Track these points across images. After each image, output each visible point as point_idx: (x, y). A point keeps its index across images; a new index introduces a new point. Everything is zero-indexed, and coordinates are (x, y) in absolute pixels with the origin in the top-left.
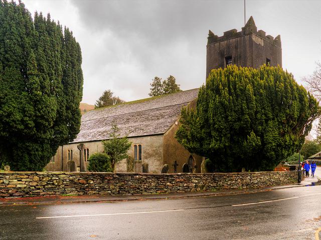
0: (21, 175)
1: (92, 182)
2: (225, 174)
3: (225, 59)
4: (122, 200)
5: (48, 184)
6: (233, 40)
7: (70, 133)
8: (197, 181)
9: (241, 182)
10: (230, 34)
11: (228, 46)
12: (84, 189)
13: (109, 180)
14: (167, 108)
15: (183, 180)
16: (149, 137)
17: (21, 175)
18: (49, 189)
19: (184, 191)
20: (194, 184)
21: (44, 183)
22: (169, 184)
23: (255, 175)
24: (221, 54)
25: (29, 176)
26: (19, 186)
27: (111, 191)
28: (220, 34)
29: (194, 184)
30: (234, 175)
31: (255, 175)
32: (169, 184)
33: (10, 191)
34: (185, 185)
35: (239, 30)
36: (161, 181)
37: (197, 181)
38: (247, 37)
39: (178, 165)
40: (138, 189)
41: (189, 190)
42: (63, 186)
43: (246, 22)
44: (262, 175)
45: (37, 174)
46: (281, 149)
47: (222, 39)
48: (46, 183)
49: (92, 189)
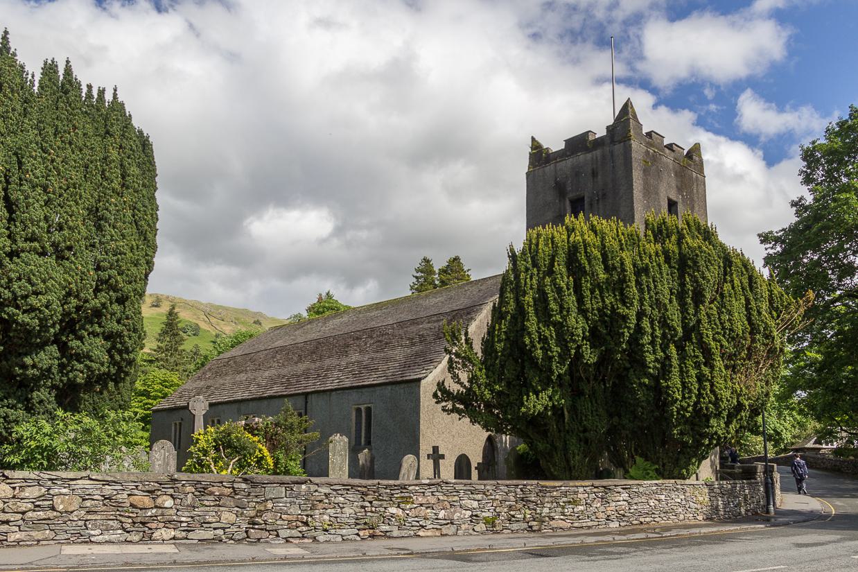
2: (557, 483)
3: (568, 203)
4: (126, 564)
6: (582, 157)
7: (113, 362)
8: (475, 504)
9: (602, 509)
10: (578, 144)
11: (577, 172)
12: (143, 524)
13: (220, 497)
14: (435, 318)
15: (433, 500)
16: (389, 388)
18: (36, 524)
19: (438, 533)
20: (469, 513)
21: (24, 506)
22: (393, 510)
23: (641, 489)
24: (560, 189)
27: (224, 529)
28: (555, 144)
29: (469, 513)
30: (583, 489)
31: (641, 489)
32: (393, 510)
34: (442, 514)
35: (601, 132)
36: (371, 502)
37: (475, 504)
38: (618, 148)
39: (442, 457)
40: (306, 524)
41: (452, 529)
42: (83, 512)
43: (617, 113)
44: (662, 489)
45: (7, 478)
46: (6, 168)
47: (561, 155)
48: (30, 506)
49: (168, 523)
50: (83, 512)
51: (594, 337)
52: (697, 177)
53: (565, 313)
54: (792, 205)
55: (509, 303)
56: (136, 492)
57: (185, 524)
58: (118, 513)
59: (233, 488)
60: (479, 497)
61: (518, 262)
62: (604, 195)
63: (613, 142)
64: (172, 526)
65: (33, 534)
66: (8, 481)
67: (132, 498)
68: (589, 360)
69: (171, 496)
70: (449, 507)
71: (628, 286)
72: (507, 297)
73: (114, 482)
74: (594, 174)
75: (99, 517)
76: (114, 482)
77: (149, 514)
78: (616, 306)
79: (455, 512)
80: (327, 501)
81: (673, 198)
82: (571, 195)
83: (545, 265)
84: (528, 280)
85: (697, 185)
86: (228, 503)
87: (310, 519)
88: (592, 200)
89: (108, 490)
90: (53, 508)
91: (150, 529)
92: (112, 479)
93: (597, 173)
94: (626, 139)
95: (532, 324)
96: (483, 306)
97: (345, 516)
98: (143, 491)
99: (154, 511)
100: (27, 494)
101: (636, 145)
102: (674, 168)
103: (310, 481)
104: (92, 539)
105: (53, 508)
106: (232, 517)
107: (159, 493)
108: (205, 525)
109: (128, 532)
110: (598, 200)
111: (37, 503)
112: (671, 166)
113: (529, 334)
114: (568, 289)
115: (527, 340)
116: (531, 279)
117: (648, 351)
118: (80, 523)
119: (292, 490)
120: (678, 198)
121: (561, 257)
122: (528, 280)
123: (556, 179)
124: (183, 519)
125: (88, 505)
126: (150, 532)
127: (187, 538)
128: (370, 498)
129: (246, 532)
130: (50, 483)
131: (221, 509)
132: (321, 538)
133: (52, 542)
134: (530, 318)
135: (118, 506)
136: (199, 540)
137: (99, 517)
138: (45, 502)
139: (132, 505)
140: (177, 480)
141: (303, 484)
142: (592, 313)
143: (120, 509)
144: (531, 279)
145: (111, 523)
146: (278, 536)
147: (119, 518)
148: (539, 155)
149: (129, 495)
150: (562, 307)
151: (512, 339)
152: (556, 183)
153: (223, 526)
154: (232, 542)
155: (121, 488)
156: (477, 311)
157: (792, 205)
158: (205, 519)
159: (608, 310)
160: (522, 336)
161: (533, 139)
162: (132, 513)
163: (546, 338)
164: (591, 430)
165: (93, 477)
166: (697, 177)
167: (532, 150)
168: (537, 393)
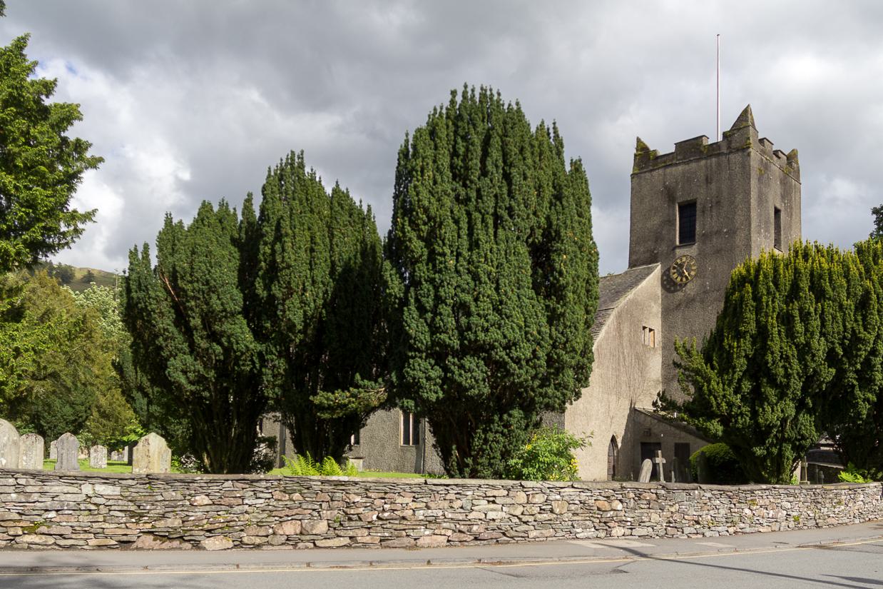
0: (493, 487)
1: (620, 506)
5: (542, 510)
10: (691, 149)
15: (767, 502)
17: (493, 487)
18: (543, 524)
25: (509, 490)
26: (491, 515)
28: (663, 145)
33: (475, 528)
36: (735, 504)
50: (570, 515)
51: (831, 358)
52: (795, 185)
53: (808, 335)
54: (874, 213)
55: (749, 323)
56: (601, 498)
57: (629, 524)
58: (591, 515)
59: (656, 494)
60: (791, 499)
61: (760, 286)
62: (718, 202)
63: (731, 150)
64: (622, 525)
65: (543, 531)
66: (525, 490)
67: (597, 502)
68: (825, 378)
69: (620, 501)
70: (775, 507)
71: (872, 314)
72: (746, 318)
73: (588, 490)
74: (708, 180)
75: (580, 518)
76: (588, 490)
77: (609, 515)
78: (857, 331)
79: (779, 512)
80: (709, 504)
81: (779, 207)
82: (681, 200)
83: (785, 290)
84: (770, 303)
85: (795, 192)
86: (655, 506)
87: (700, 519)
88: (704, 207)
89: (583, 496)
90: (552, 511)
91: (609, 527)
92: (586, 487)
93: (711, 179)
94: (744, 149)
95: (777, 343)
96: (609, 312)
97: (720, 516)
98: (604, 497)
99: (612, 513)
100: (537, 500)
101: (754, 152)
102: (780, 175)
103: (700, 488)
104: (578, 536)
105: (552, 511)
106: (658, 519)
107: (614, 498)
108: (642, 524)
109: (597, 530)
110: (711, 207)
111: (543, 507)
112: (777, 174)
113: (772, 353)
114: (816, 314)
115: (770, 359)
116: (773, 302)
117: (877, 371)
118: (570, 523)
119: (690, 495)
120: (782, 206)
121: (805, 284)
122: (770, 303)
123: (665, 183)
124: (629, 519)
125: (573, 508)
126: (610, 530)
127: (631, 535)
128: (734, 501)
129: (666, 529)
130: (548, 490)
131: (651, 511)
132: (708, 534)
133: (554, 539)
134: (774, 339)
135: (590, 509)
136: (639, 536)
137: (580, 518)
138: (547, 508)
139: (599, 509)
140: (625, 488)
141: (695, 490)
142: (832, 336)
143: (592, 512)
144: (773, 302)
145: (587, 522)
146: (683, 532)
147: (592, 519)
148: (645, 158)
149: (595, 500)
150: (807, 330)
151: (750, 356)
152: (666, 187)
153: (652, 524)
154: (658, 537)
155: (590, 494)
156: (604, 316)
157: (874, 213)
158: (642, 519)
159: (848, 333)
160: (765, 354)
161: (638, 140)
162: (598, 514)
163: (787, 357)
164: (808, 438)
165: (576, 486)
166: (795, 185)
167: (637, 150)
168: (772, 406)
